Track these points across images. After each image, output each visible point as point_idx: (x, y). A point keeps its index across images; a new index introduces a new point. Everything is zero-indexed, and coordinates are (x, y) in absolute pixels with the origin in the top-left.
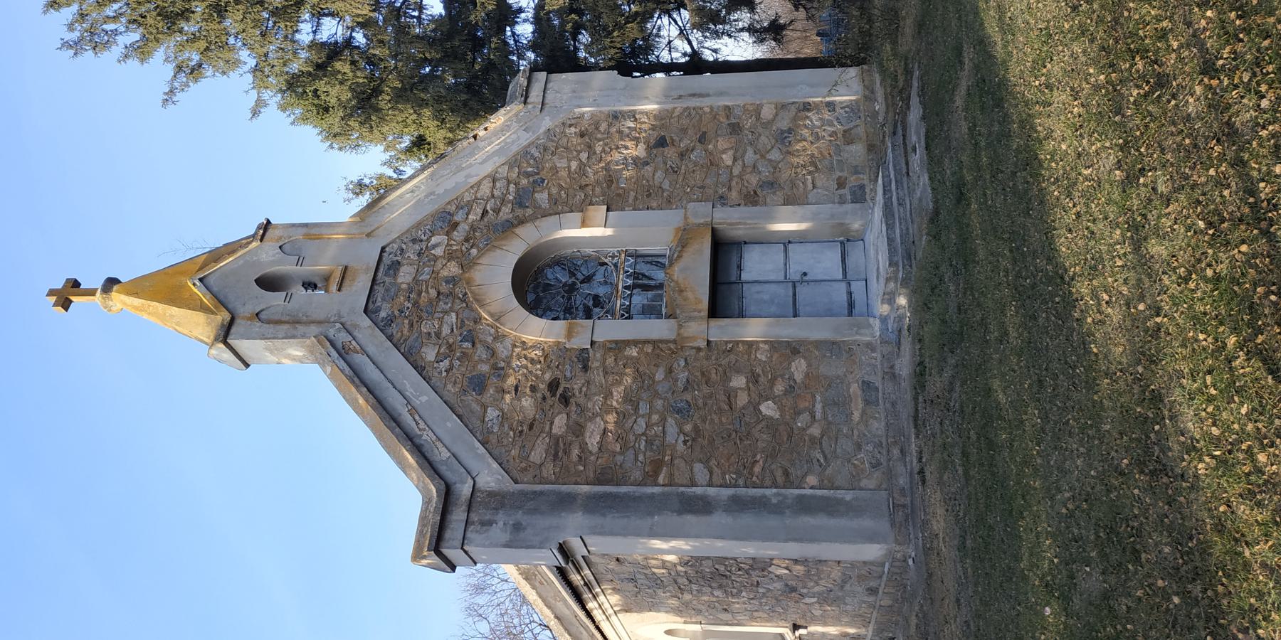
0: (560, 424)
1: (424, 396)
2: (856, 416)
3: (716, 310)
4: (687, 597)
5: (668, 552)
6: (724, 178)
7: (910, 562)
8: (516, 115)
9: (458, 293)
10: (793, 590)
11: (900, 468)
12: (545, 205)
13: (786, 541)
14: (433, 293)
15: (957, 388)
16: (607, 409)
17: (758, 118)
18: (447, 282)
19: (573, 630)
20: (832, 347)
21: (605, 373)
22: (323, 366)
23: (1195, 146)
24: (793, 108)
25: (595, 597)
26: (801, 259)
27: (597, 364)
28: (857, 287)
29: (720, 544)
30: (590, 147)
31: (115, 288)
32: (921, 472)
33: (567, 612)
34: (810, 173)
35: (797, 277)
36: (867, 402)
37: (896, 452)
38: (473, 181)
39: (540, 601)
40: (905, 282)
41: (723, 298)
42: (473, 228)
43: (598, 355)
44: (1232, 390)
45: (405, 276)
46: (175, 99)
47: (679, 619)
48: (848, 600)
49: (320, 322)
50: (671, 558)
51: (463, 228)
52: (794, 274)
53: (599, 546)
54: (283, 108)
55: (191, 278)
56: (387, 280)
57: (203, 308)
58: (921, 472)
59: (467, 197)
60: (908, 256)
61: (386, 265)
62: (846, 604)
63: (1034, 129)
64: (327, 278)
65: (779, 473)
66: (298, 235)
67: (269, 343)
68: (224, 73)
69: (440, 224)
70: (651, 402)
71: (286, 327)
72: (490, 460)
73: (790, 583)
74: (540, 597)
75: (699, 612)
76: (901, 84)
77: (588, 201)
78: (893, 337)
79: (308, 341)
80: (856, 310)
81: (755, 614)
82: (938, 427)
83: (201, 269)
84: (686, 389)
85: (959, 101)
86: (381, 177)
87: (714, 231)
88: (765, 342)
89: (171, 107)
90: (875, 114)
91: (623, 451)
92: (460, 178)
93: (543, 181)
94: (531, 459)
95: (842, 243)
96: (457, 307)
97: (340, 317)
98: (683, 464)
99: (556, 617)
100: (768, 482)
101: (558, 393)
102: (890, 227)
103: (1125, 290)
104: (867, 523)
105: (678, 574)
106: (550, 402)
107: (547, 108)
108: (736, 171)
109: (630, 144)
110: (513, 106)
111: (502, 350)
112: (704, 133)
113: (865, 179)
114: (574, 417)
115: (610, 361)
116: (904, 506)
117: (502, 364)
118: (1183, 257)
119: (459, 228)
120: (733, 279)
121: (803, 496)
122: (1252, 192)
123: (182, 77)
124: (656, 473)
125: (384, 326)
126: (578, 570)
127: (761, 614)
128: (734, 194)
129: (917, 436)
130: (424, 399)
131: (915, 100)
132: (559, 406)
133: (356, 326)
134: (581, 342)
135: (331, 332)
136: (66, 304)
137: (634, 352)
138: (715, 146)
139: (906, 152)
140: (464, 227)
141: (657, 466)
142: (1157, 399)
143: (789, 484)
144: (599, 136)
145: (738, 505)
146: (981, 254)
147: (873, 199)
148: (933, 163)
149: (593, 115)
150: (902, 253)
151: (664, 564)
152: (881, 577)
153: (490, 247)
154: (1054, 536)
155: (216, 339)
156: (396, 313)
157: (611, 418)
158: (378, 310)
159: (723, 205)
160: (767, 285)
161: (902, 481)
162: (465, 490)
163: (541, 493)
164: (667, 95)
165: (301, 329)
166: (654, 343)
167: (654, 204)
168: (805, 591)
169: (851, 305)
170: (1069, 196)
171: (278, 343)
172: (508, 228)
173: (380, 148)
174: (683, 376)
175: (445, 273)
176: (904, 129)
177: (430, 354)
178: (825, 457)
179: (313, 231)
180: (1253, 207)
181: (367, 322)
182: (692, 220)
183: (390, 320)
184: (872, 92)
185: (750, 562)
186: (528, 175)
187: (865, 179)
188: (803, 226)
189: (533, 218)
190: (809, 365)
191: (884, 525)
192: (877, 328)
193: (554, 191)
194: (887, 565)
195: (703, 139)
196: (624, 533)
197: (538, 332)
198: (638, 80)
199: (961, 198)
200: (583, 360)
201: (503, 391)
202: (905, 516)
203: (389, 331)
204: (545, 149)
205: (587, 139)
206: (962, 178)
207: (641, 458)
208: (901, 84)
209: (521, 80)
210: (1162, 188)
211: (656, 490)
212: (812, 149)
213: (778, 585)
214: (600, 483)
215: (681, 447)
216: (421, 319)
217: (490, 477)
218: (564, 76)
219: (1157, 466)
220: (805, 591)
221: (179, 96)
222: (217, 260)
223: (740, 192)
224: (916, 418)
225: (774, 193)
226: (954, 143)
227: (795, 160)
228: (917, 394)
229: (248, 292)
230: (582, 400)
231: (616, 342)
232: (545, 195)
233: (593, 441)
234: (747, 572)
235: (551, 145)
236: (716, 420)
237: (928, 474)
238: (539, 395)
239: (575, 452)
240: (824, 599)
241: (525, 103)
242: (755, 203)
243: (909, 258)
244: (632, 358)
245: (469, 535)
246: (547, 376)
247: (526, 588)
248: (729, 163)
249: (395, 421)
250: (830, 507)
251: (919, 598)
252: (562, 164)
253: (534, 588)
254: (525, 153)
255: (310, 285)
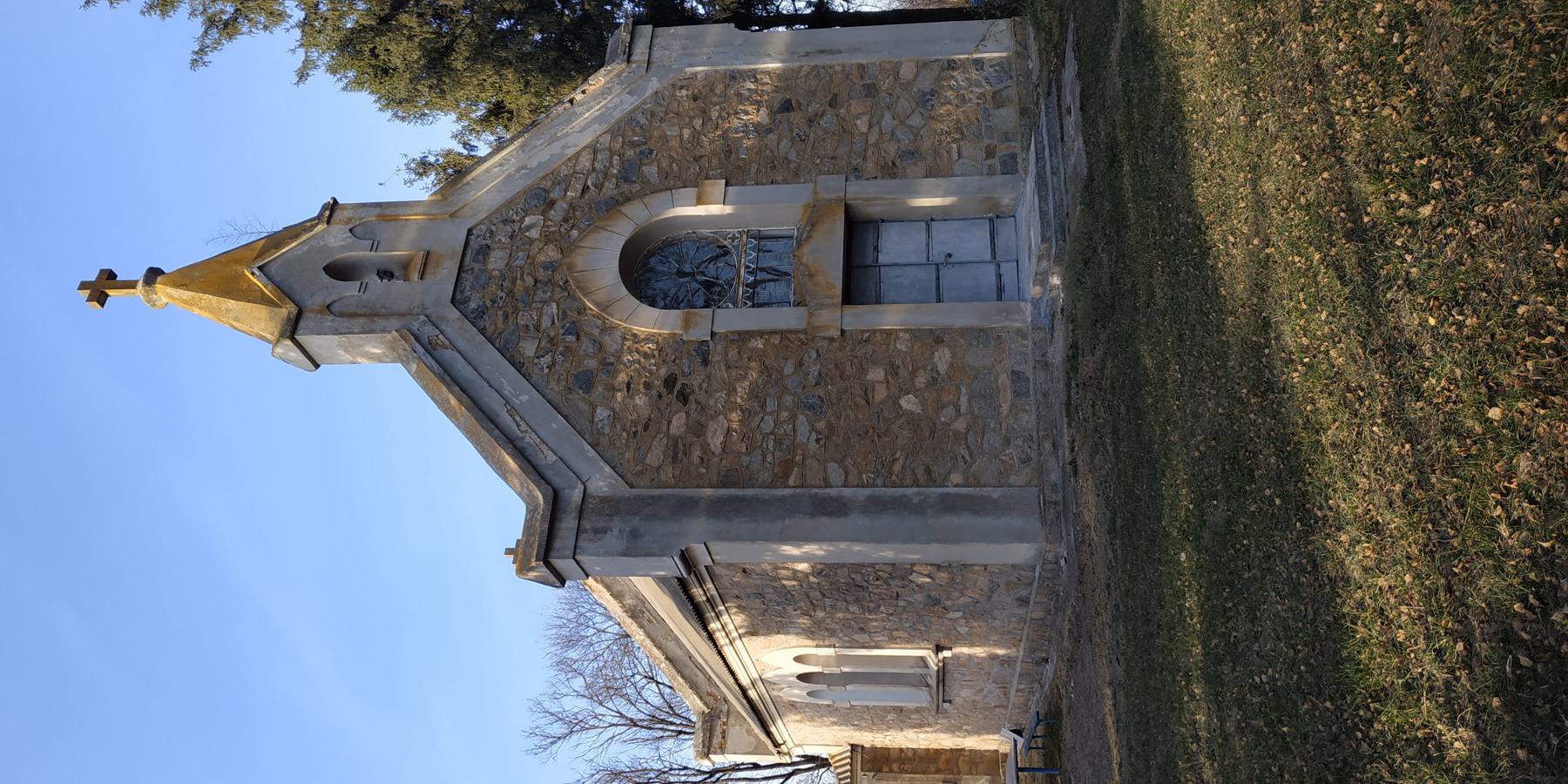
0: (678, 423)
1: (525, 396)
2: (1005, 408)
3: (851, 296)
4: (820, 614)
5: (800, 559)
6: (858, 147)
7: (1062, 562)
8: (618, 76)
9: (559, 281)
10: (936, 602)
11: (1052, 463)
12: (654, 179)
13: (928, 542)
14: (529, 281)
15: (1109, 364)
16: (730, 406)
17: (897, 77)
18: (545, 268)
19: (687, 672)
20: (979, 335)
21: (728, 367)
22: (406, 364)
23: (1295, 87)
24: (936, 67)
25: (718, 615)
26: (945, 238)
27: (717, 358)
28: (1008, 269)
29: (856, 548)
30: (704, 112)
31: (159, 279)
32: (1073, 462)
33: (680, 653)
34: (955, 141)
35: (941, 259)
36: (1017, 394)
37: (1047, 446)
38: (570, 152)
39: (648, 641)
40: (1058, 260)
41: (858, 284)
42: (572, 207)
43: (719, 348)
44: (1317, 301)
45: (496, 261)
46: (206, 59)
47: (810, 642)
48: (996, 613)
49: (400, 315)
50: (803, 567)
51: (563, 203)
52: (937, 254)
53: (724, 553)
54: (333, 70)
55: (249, 267)
56: (476, 266)
57: (264, 300)
58: (1073, 462)
59: (564, 171)
60: (1063, 230)
61: (474, 250)
62: (994, 618)
63: (1178, 80)
64: (406, 265)
65: (920, 472)
66: (371, 216)
67: (344, 339)
68: (266, 28)
69: (535, 202)
70: (779, 399)
71: (362, 320)
72: (602, 463)
73: (933, 594)
74: (648, 635)
75: (833, 633)
76: (1056, 38)
77: (703, 175)
78: (1046, 322)
79: (388, 337)
80: (1006, 295)
81: (895, 634)
82: (1090, 410)
83: (260, 255)
84: (818, 383)
85: (1114, 56)
86: (449, 153)
87: (847, 207)
88: (906, 331)
89: (201, 69)
90: (1028, 74)
91: (750, 450)
92: (555, 149)
93: (651, 152)
94: (648, 461)
95: (991, 220)
96: (557, 296)
97: (423, 306)
98: (816, 464)
99: (667, 658)
100: (908, 481)
101: (675, 389)
102: (1042, 198)
103: (1245, 229)
104: (1015, 521)
105: (810, 585)
106: (666, 399)
107: (653, 67)
108: (872, 139)
109: (750, 109)
110: (614, 65)
111: (611, 343)
112: (835, 95)
113: (1016, 146)
114: (694, 415)
115: (733, 354)
116: (1056, 503)
117: (612, 359)
118: (1286, 189)
119: (557, 206)
120: (869, 262)
121: (947, 494)
122: (1331, 125)
123: (214, 33)
124: (787, 475)
125: (476, 318)
126: (701, 583)
127: (901, 634)
128: (870, 165)
129: (1069, 425)
130: (525, 398)
131: (1070, 55)
132: (676, 405)
133: (443, 318)
134: (700, 333)
135: (415, 326)
136: (101, 299)
137: (759, 344)
138: (848, 111)
139: (1060, 113)
140: (562, 206)
141: (787, 466)
142: (1266, 324)
143: (931, 481)
144: (715, 99)
145: (876, 506)
146: (1133, 217)
147: (1026, 170)
148: (1088, 125)
149: (707, 74)
150: (1055, 227)
151: (795, 575)
152: (1031, 584)
153: (592, 227)
154: (1188, 483)
155: (282, 335)
156: (488, 303)
157: (735, 416)
158: (467, 300)
159: (858, 178)
160: (907, 269)
161: (1054, 477)
162: (576, 495)
163: (660, 497)
164: (791, 52)
165: (381, 322)
166: (783, 334)
167: (779, 178)
168: (949, 603)
169: (1000, 290)
170: (1206, 145)
171: (354, 338)
172: (613, 206)
173: (453, 116)
174: (814, 369)
175: (542, 258)
176: (1059, 89)
177: (529, 348)
178: (971, 455)
179: (388, 212)
180: (1332, 138)
181: (454, 314)
182: (824, 195)
183: (481, 312)
184: (1026, 48)
185: (889, 569)
186: (633, 145)
187: (1016, 146)
188: (948, 201)
189: (641, 195)
190: (954, 355)
191: (1034, 524)
192: (1028, 313)
193: (664, 163)
194: (1038, 570)
195: (833, 103)
196: (753, 538)
197: (650, 323)
198: (753, 35)
199: (1114, 160)
200: (703, 353)
201: (614, 389)
202: (1057, 513)
203: (481, 324)
204: (653, 114)
205: (700, 102)
206: (1115, 138)
207: (769, 458)
208: (1056, 38)
209: (623, 34)
210: (1272, 128)
211: (786, 492)
212: (958, 114)
213: (919, 597)
214: (725, 486)
215: (813, 446)
216: (516, 310)
217: (602, 481)
218: (672, 30)
219: (1267, 387)
220: (949, 603)
221: (211, 56)
222: (278, 246)
223: (876, 163)
224: (1068, 404)
225: (915, 164)
226: (1109, 103)
227: (939, 126)
228: (1069, 378)
229: (314, 282)
230: (702, 397)
231: (739, 333)
232: (654, 168)
233: (716, 441)
234: (886, 582)
235: (660, 111)
236: (852, 416)
237: (1080, 462)
238: (654, 392)
239: (697, 453)
240: (971, 613)
241: (628, 61)
242: (894, 176)
243: (1063, 232)
244: (757, 350)
245: (581, 543)
246: (663, 372)
247: (631, 627)
248: (864, 129)
249: (493, 421)
250: (976, 506)
251: (1072, 601)
252: (672, 132)
253: (641, 626)
254: (630, 119)
255: (385, 274)
